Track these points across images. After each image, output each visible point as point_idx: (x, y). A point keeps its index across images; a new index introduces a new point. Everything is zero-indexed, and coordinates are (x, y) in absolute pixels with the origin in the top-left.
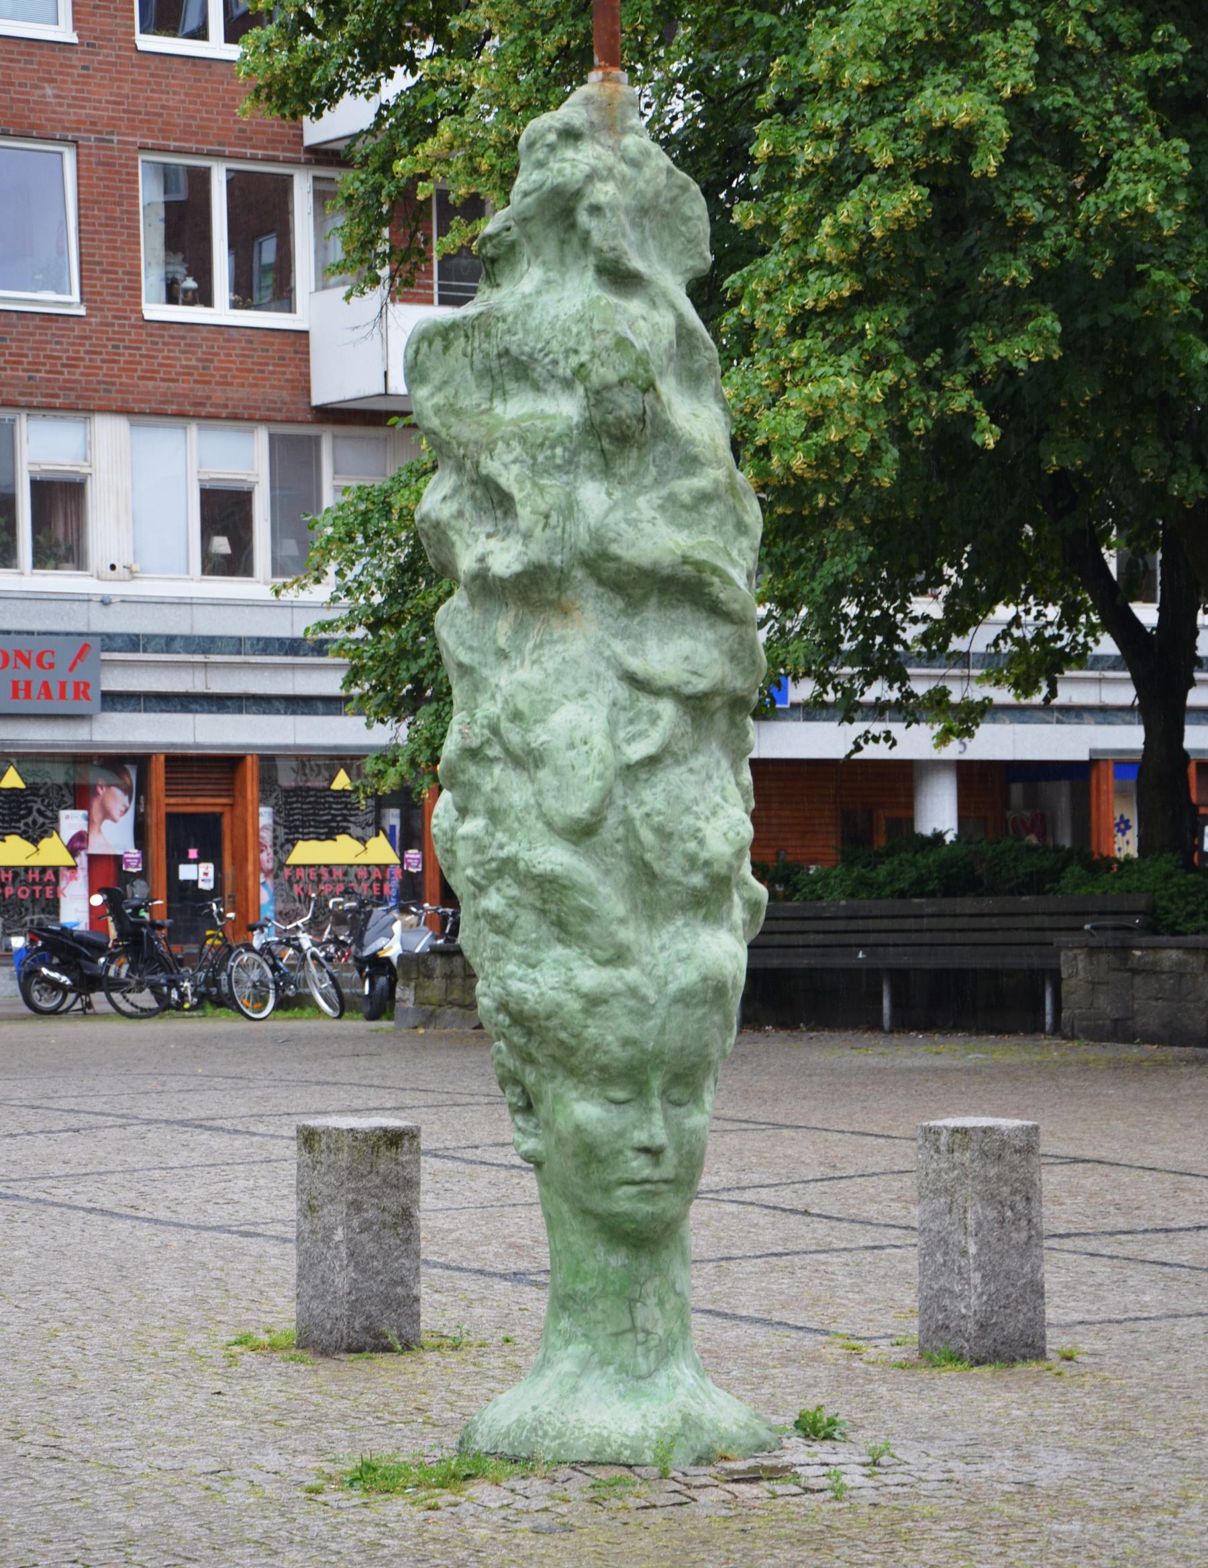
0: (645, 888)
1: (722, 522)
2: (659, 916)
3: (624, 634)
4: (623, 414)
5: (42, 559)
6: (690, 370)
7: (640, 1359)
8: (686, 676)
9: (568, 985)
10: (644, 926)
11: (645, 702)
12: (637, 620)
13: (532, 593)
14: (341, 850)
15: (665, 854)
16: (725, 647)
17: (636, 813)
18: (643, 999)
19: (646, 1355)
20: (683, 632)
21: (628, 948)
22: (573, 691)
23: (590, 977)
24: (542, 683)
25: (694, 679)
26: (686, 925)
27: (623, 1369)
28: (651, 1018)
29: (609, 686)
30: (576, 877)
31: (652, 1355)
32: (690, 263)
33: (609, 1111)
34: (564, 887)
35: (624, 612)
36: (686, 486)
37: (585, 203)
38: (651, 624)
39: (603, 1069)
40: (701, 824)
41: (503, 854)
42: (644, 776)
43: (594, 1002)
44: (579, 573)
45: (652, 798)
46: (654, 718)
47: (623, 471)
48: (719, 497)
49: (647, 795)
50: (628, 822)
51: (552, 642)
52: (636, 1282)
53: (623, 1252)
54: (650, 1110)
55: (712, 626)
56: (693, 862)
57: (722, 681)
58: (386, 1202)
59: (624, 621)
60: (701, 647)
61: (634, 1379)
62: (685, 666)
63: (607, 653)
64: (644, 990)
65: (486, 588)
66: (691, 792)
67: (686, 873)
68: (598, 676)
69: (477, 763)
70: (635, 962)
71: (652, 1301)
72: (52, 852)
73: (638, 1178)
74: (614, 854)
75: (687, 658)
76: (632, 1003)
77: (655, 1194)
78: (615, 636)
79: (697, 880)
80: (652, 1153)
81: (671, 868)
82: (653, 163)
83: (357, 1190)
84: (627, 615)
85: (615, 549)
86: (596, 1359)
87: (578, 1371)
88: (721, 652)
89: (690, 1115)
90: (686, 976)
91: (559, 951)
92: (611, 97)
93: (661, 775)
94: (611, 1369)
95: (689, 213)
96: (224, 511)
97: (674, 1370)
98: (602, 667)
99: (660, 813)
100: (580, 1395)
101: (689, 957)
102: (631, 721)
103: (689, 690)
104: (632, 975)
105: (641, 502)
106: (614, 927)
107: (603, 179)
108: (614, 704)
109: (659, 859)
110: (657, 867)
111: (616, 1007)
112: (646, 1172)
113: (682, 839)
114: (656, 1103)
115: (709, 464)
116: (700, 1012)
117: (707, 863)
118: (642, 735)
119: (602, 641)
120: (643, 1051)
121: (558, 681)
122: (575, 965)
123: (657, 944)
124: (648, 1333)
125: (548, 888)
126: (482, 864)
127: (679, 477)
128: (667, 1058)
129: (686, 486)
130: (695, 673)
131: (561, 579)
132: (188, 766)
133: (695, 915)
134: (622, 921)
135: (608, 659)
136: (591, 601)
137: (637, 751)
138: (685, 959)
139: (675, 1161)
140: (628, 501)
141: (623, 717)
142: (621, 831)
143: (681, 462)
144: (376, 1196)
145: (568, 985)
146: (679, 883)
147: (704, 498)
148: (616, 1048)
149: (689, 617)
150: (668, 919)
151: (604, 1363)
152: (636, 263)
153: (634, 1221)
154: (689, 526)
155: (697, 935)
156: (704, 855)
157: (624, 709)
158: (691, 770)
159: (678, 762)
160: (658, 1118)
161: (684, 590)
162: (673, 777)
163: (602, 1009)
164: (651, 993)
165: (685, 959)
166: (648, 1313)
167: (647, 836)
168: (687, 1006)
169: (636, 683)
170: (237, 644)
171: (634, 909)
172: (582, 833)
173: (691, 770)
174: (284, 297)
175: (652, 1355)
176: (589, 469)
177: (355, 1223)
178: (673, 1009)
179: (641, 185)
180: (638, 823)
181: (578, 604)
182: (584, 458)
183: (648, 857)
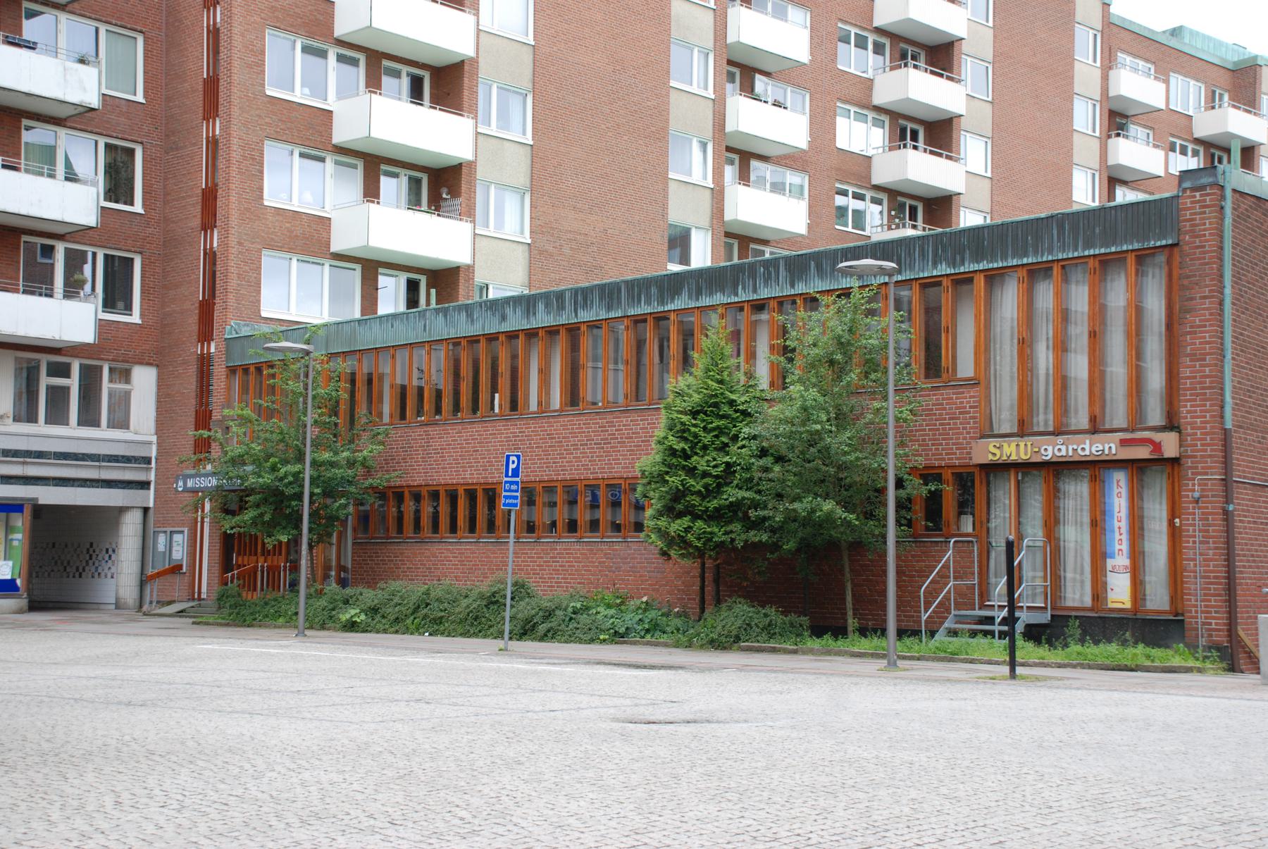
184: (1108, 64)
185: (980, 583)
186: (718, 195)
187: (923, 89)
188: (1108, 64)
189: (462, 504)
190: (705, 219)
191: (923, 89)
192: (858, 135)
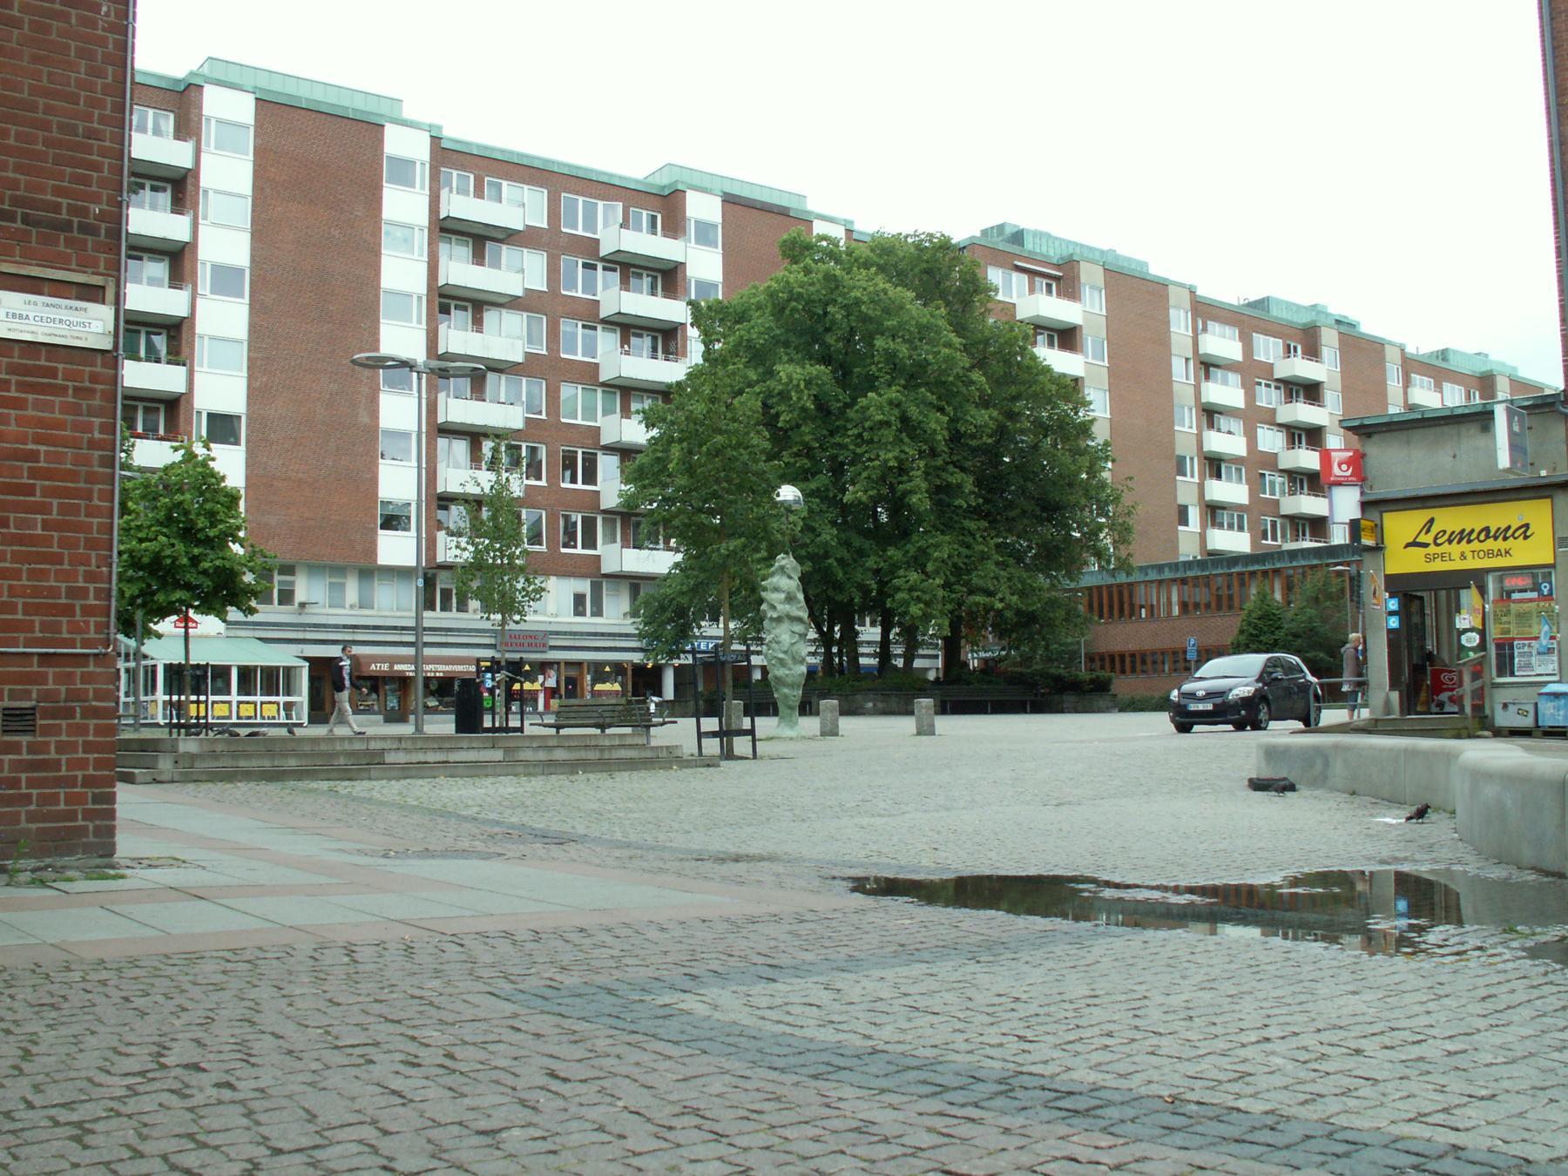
5: (442, 609)
13: (779, 620)
14: (607, 687)
61: (792, 727)
65: (772, 619)
72: (537, 686)
96: (579, 599)
125: (781, 660)
132: (569, 664)
161: (799, 620)
170: (582, 634)
172: (785, 652)
174: (594, 547)
184: (1407, 383)
185: (56, 386)
186: (1201, 487)
187: (1304, 413)
188: (1407, 383)
189: (1128, 660)
190: (1195, 500)
191: (1304, 413)
192: (1271, 441)
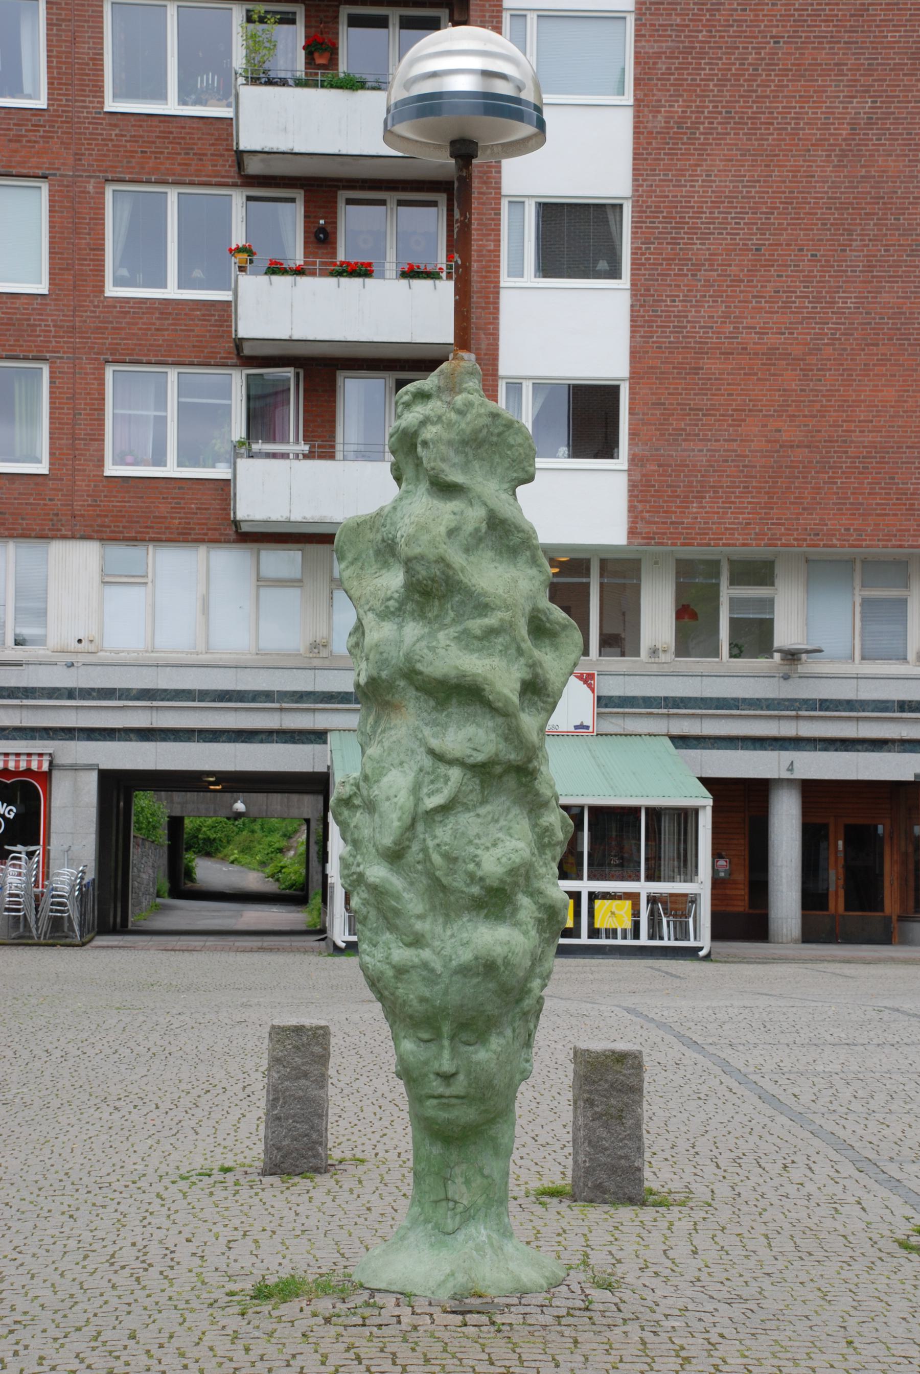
0: (441, 895)
1: (507, 648)
2: (452, 914)
3: (435, 723)
4: (420, 577)
6: (508, 546)
7: (449, 1221)
8: (469, 752)
9: (387, 959)
10: (441, 920)
11: (442, 769)
12: (445, 713)
15: (452, 872)
16: (500, 732)
17: (431, 843)
18: (432, 971)
19: (453, 1218)
20: (474, 722)
21: (423, 936)
22: (396, 762)
23: (401, 954)
24: (381, 756)
25: (475, 754)
26: (469, 921)
27: (437, 1226)
28: (438, 984)
29: (419, 758)
30: (387, 886)
31: (458, 1218)
32: (515, 475)
33: (419, 1046)
34: (382, 893)
35: (435, 709)
36: (477, 624)
37: (419, 440)
38: (455, 716)
39: (411, 1017)
40: (479, 852)
41: (358, 870)
42: (440, 819)
43: (401, 971)
44: (402, 683)
45: (443, 833)
46: (447, 779)
47: (430, 615)
48: (505, 630)
49: (439, 832)
50: (425, 850)
51: (390, 728)
52: (448, 1166)
53: (439, 1144)
54: (442, 1047)
55: (493, 717)
56: (472, 878)
57: (497, 755)
58: (613, 1101)
59: (435, 715)
60: (481, 732)
62: (468, 744)
63: (420, 736)
64: (433, 964)
66: (473, 831)
67: (468, 885)
68: (412, 751)
69: (349, 809)
70: (428, 945)
71: (459, 1180)
73: (436, 1094)
74: (417, 872)
75: (470, 739)
76: (424, 973)
77: (449, 1105)
78: (426, 724)
79: (475, 890)
80: (447, 1078)
81: (458, 882)
82: (474, 411)
83: (590, 1092)
84: (437, 711)
85: (419, 666)
86: (422, 1218)
87: (409, 1225)
88: (497, 735)
89: (476, 1052)
90: (466, 956)
91: (387, 936)
92: (454, 370)
93: (452, 819)
94: (430, 1226)
95: (512, 442)
97: (471, 1230)
98: (415, 745)
99: (446, 844)
100: (406, 1242)
101: (467, 943)
102: (432, 782)
103: (471, 761)
104: (426, 954)
105: (441, 635)
106: (413, 920)
107: (434, 423)
108: (421, 770)
109: (447, 875)
110: (444, 881)
111: (414, 976)
112: (441, 1090)
113: (464, 862)
114: (446, 1043)
115: (499, 608)
116: (475, 980)
117: (482, 879)
118: (438, 791)
119: (418, 728)
120: (434, 1007)
121: (389, 754)
122: (393, 945)
123: (449, 933)
124: (456, 1202)
126: (348, 876)
127: (474, 618)
128: (450, 1011)
129: (477, 624)
130: (475, 750)
131: (390, 686)
133: (478, 915)
134: (420, 917)
135: (420, 740)
136: (412, 701)
137: (431, 803)
138: (465, 944)
139: (465, 1083)
140: (432, 635)
141: (427, 779)
142: (421, 856)
143: (475, 608)
144: (605, 1096)
145: (387, 959)
146: (462, 892)
147: (491, 632)
148: (415, 1003)
149: (479, 712)
150: (459, 916)
151: (427, 1221)
152: (456, 477)
153: (437, 1124)
154: (480, 650)
155: (476, 928)
156: (480, 873)
157: (428, 773)
158: (478, 815)
159: (468, 810)
160: (446, 1054)
162: (467, 822)
163: (405, 977)
164: (438, 967)
165: (465, 944)
166: (458, 1189)
167: (437, 859)
168: (465, 976)
169: (438, 756)
171: (433, 908)
173: (478, 815)
175: (458, 1218)
176: (412, 613)
177: (589, 1114)
178: (454, 978)
179: (463, 425)
180: (431, 851)
181: (404, 703)
182: (409, 607)
183: (438, 873)
